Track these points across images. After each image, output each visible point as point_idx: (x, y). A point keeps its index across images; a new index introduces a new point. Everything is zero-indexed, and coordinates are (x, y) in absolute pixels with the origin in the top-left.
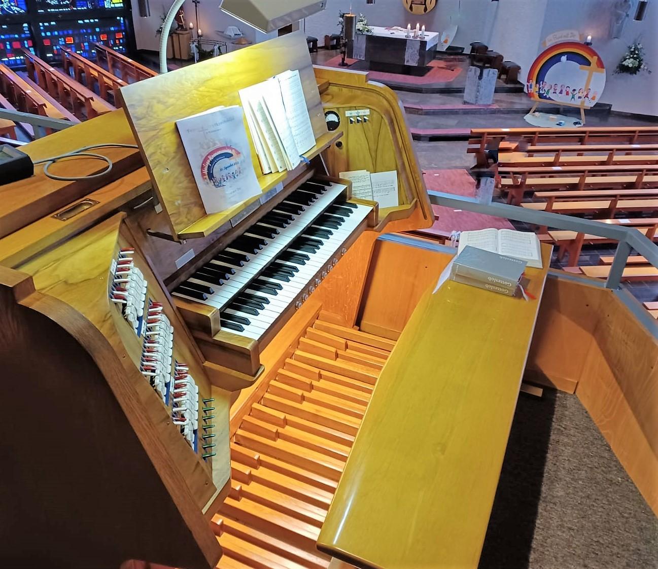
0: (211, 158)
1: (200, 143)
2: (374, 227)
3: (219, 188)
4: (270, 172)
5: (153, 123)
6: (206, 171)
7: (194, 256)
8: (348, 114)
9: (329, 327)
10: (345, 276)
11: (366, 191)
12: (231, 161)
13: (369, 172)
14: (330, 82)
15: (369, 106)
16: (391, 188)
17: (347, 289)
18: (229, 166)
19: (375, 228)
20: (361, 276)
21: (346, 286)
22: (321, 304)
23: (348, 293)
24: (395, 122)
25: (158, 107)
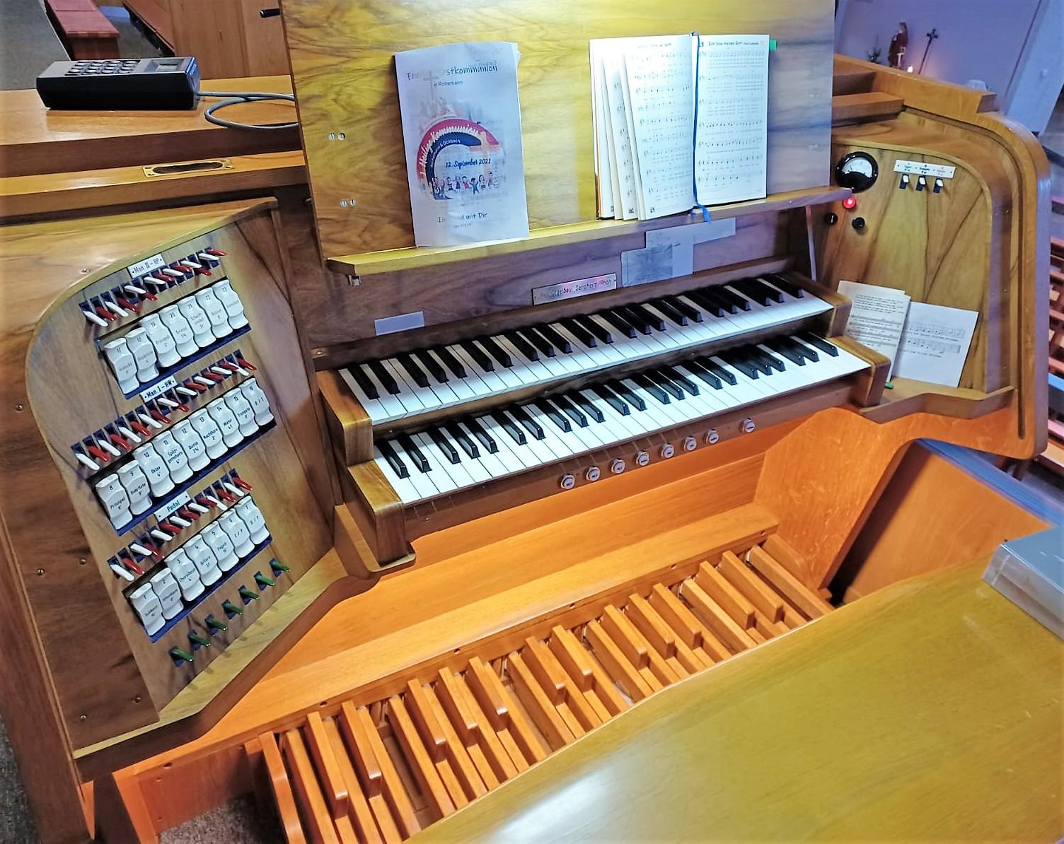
0: (435, 137)
1: (422, 104)
2: (862, 406)
3: (439, 201)
5: (336, 42)
6: (424, 162)
7: (423, 325)
8: (900, 165)
10: (830, 491)
11: (888, 333)
12: (476, 154)
13: (909, 298)
14: (905, 104)
15: (957, 160)
16: (952, 347)
17: (827, 515)
18: (467, 163)
19: (862, 410)
21: (827, 509)
22: (777, 523)
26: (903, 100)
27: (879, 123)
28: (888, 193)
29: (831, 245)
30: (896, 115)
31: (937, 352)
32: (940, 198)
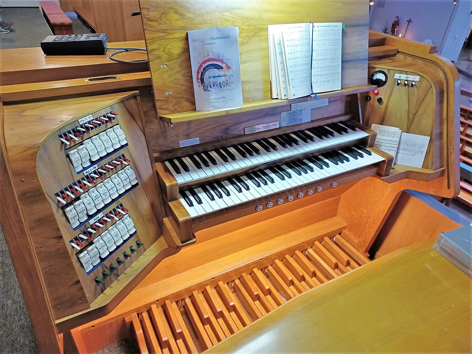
0: (204, 66)
4: (277, 98)
6: (200, 76)
8: (397, 76)
9: (344, 244)
11: (392, 146)
12: (221, 73)
13: (401, 131)
15: (421, 74)
17: (367, 222)
18: (217, 77)
19: (382, 178)
20: (380, 216)
22: (346, 225)
23: (367, 225)
24: (445, 95)
25: (173, 16)
26: (398, 49)
27: (387, 58)
28: (392, 88)
29: (368, 109)
30: (395, 55)
31: (413, 153)
32: (414, 89)
